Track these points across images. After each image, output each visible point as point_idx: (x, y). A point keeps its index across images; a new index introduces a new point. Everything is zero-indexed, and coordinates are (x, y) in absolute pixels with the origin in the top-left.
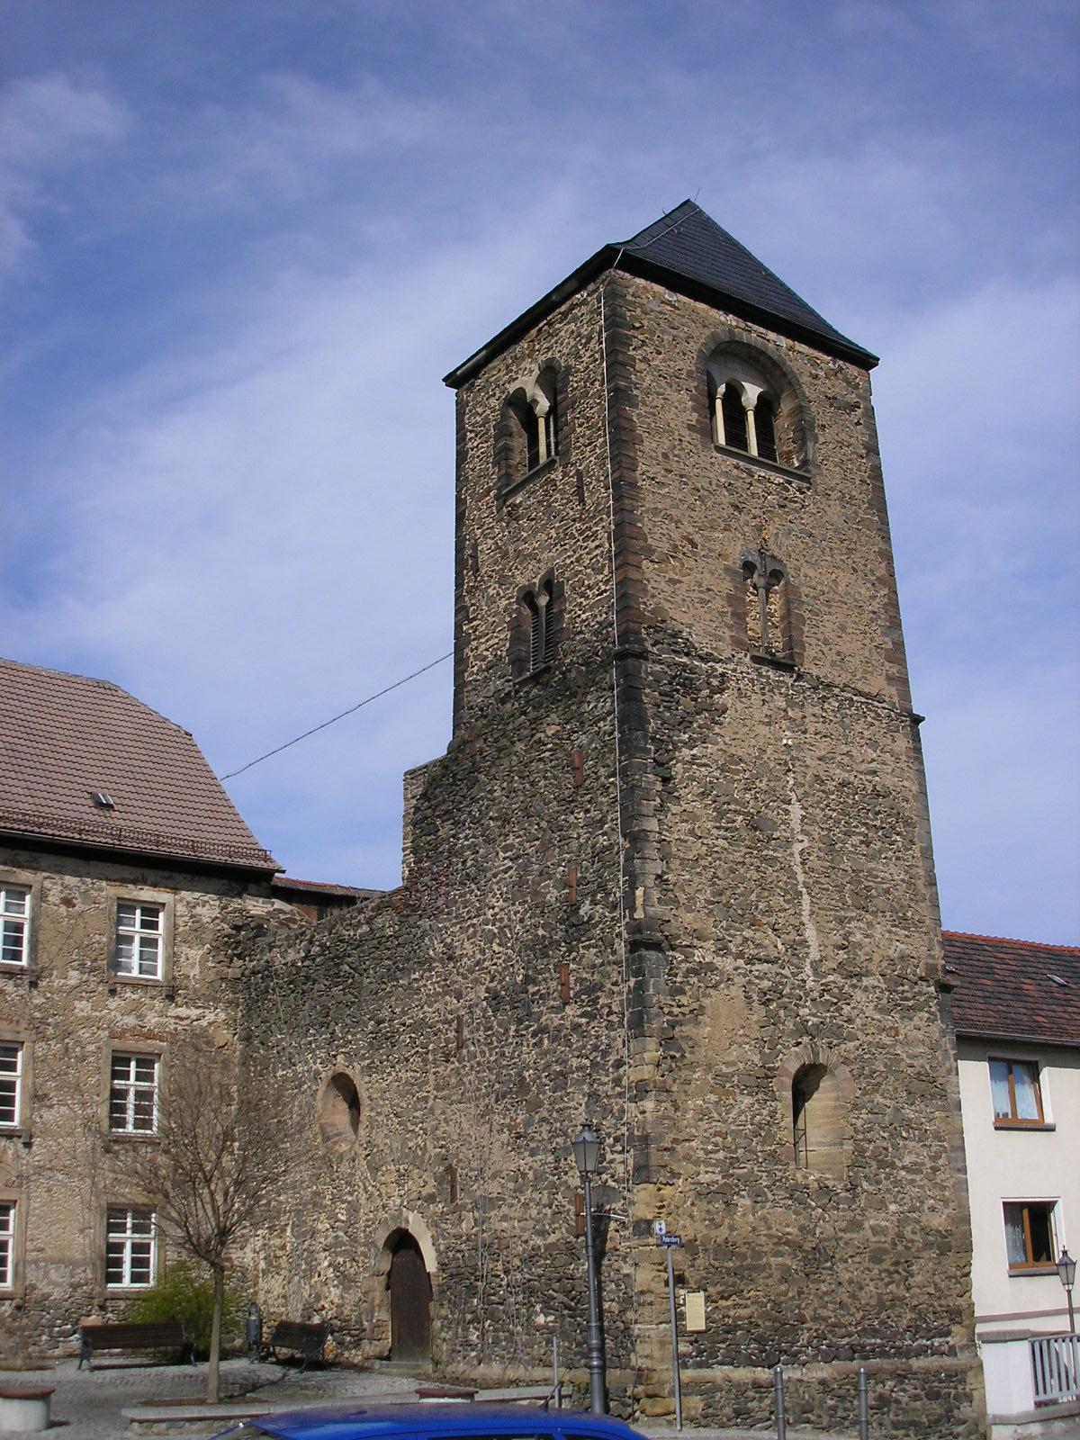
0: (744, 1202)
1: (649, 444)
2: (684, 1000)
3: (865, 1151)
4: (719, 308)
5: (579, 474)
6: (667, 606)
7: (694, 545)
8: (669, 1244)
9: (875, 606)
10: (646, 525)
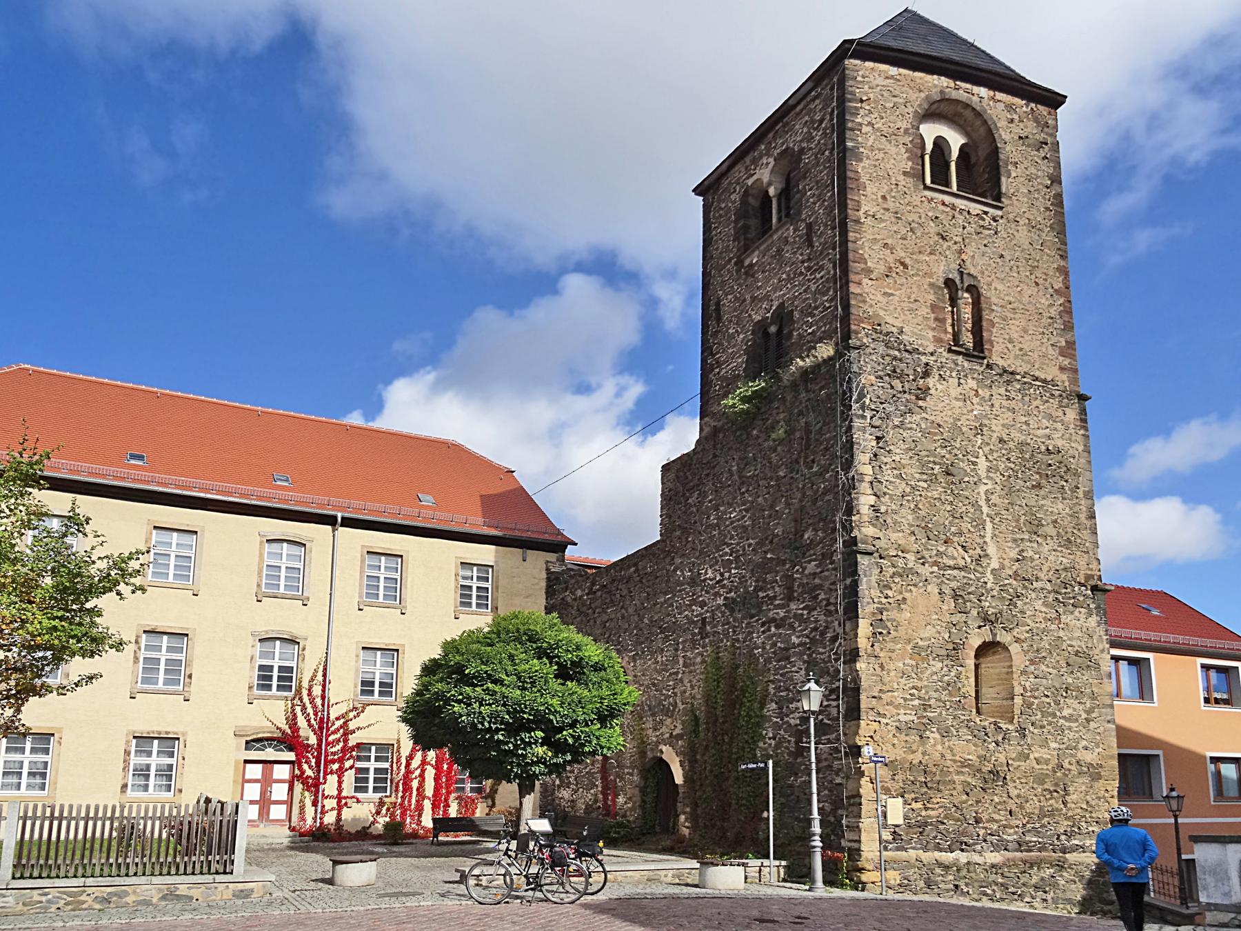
0: (933, 736)
1: (871, 189)
2: (890, 593)
3: (1033, 704)
4: (933, 73)
5: (809, 227)
6: (882, 313)
7: (905, 266)
8: (876, 762)
9: (1053, 312)
10: (866, 252)
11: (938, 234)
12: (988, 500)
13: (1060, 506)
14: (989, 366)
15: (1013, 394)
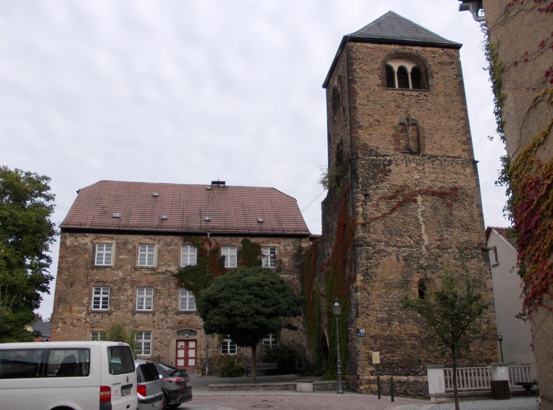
1: (361, 94)
2: (372, 261)
7: (379, 121)
10: (360, 119)
11: (396, 106)
12: (422, 215)
13: (463, 213)
14: (423, 155)
15: (436, 166)
